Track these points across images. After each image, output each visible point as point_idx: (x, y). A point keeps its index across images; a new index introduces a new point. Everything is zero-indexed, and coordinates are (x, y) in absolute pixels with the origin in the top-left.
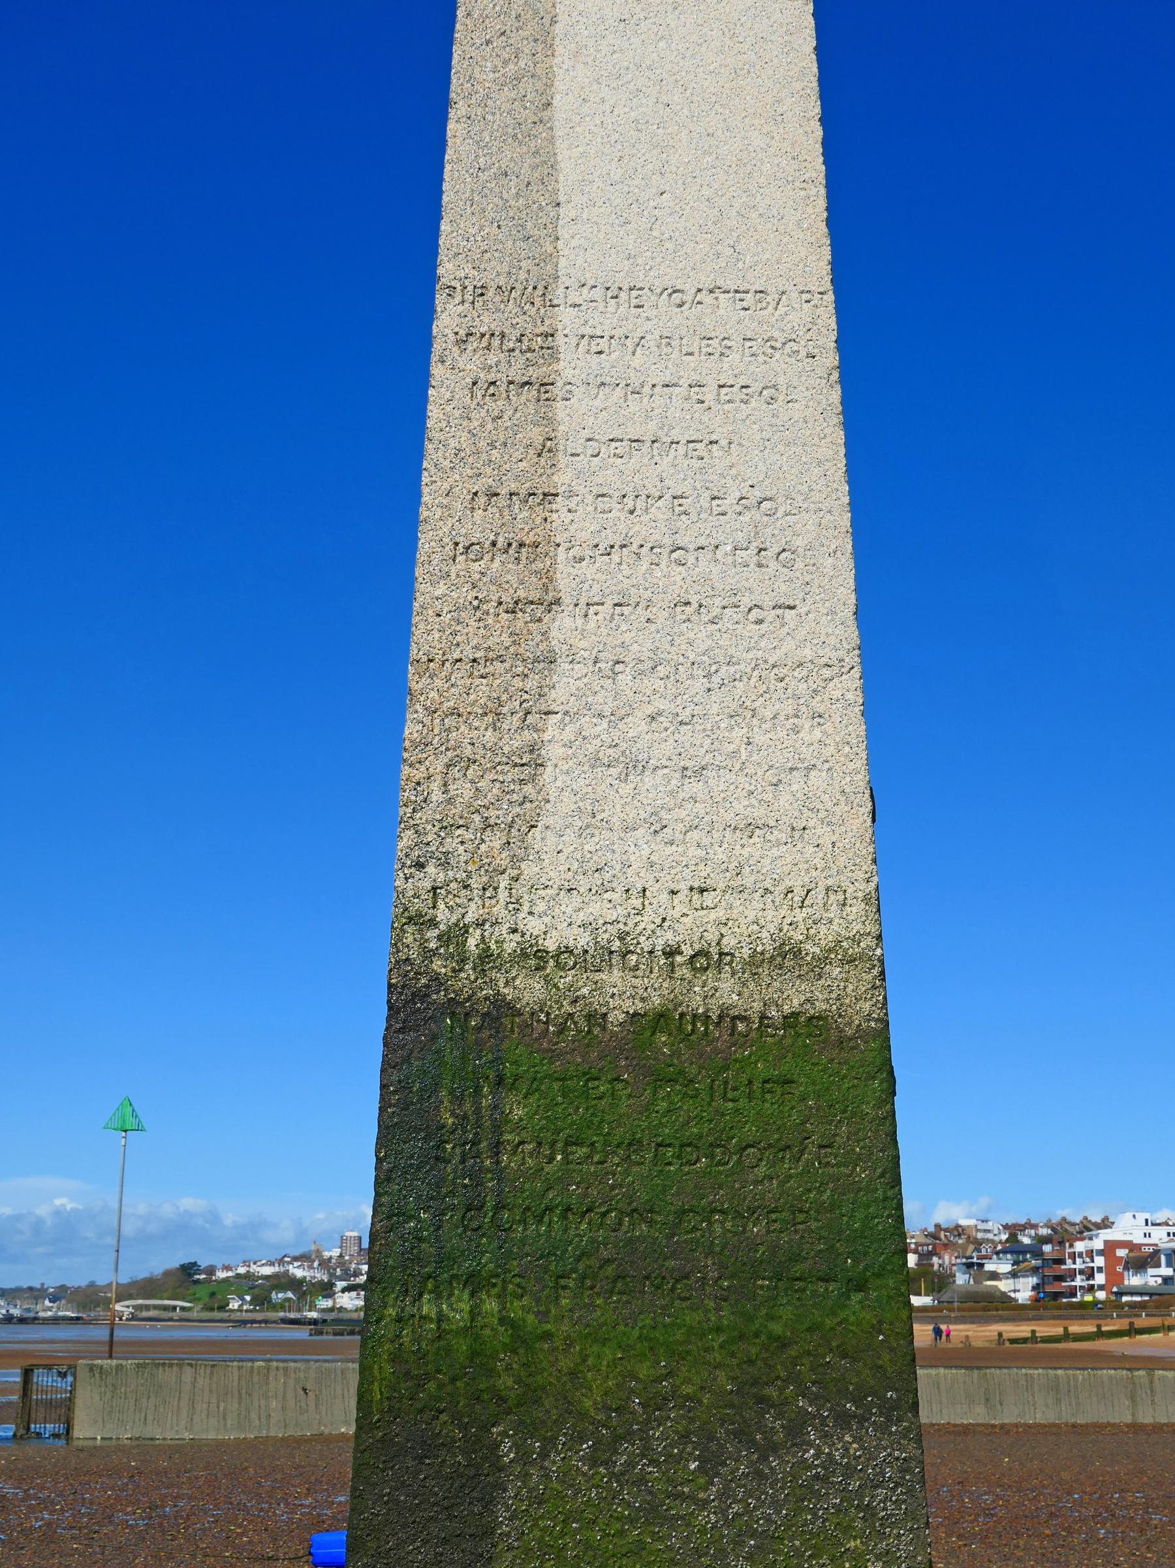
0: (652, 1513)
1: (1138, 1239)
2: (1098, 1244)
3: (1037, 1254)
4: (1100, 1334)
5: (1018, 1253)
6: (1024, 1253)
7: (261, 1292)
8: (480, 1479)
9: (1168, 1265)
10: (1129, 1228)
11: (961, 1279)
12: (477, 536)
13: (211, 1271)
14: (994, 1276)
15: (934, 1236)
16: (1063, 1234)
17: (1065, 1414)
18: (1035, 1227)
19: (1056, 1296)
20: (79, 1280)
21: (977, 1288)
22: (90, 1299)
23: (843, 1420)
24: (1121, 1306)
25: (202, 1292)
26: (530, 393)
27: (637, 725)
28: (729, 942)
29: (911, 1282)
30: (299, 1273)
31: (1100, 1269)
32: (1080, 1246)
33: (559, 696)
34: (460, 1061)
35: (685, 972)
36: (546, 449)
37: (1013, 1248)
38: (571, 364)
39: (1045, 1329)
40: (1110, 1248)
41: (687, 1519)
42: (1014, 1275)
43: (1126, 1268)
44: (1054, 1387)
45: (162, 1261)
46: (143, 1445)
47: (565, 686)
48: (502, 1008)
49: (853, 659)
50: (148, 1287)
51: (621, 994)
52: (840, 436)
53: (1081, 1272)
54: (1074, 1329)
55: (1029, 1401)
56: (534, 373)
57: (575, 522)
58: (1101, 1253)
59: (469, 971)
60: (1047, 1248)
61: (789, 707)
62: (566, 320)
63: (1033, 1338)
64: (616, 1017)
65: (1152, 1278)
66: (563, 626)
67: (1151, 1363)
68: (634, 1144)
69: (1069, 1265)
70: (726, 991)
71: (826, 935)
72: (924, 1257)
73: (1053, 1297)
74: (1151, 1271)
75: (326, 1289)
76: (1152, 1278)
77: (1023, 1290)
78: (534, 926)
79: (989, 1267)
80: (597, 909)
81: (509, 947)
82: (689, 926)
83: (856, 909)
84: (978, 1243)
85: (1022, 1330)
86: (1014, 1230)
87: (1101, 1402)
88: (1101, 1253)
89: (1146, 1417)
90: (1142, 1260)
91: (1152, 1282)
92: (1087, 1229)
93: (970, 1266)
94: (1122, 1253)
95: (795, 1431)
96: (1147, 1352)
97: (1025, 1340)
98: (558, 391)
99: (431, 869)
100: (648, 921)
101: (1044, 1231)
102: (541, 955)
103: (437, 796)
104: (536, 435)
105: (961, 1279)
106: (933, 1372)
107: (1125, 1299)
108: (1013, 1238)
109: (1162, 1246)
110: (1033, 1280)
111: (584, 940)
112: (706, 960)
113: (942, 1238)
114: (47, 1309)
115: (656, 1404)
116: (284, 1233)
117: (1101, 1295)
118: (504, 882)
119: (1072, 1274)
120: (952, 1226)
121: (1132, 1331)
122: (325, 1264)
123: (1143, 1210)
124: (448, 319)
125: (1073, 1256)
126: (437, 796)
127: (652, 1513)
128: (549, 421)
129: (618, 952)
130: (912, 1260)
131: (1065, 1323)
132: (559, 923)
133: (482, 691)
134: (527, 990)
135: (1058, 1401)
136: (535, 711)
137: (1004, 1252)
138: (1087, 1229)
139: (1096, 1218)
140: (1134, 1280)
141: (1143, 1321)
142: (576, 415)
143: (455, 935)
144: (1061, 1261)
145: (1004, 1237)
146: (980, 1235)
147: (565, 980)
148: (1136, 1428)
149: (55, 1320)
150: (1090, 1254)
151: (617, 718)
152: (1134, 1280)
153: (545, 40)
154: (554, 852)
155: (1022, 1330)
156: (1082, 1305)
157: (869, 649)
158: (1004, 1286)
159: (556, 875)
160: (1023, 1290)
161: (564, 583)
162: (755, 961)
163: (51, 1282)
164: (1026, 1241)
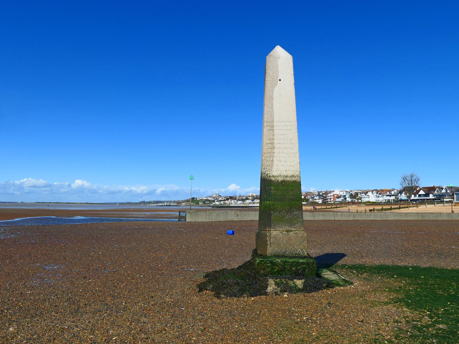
0: (283, 217)
1: (338, 194)
2: (332, 194)
3: (322, 196)
4: (332, 208)
7: (204, 202)
8: (270, 215)
10: (337, 192)
13: (196, 199)
14: (316, 199)
16: (326, 193)
19: (325, 202)
20: (177, 200)
22: (179, 203)
25: (195, 202)
27: (281, 158)
29: (303, 200)
30: (210, 199)
32: (329, 195)
33: (275, 156)
34: (266, 183)
36: (273, 135)
37: (319, 195)
38: (275, 128)
39: (323, 207)
40: (334, 195)
44: (323, 215)
45: (189, 197)
46: (196, 222)
47: (275, 155)
48: (271, 180)
50: (188, 201)
51: (280, 179)
54: (328, 207)
55: (319, 217)
57: (276, 141)
62: (275, 124)
63: (321, 208)
65: (340, 200)
66: (275, 150)
67: (337, 212)
68: (281, 190)
70: (288, 179)
71: (296, 174)
72: (305, 197)
73: (325, 202)
75: (214, 201)
76: (340, 200)
77: (320, 201)
80: (278, 172)
82: (285, 174)
84: (313, 194)
85: (320, 207)
86: (319, 192)
87: (330, 217)
89: (336, 219)
90: (339, 197)
92: (330, 192)
94: (336, 196)
95: (293, 211)
101: (324, 193)
105: (311, 200)
108: (319, 194)
112: (287, 176)
113: (307, 194)
114: (172, 204)
115: (283, 209)
116: (209, 193)
117: (332, 202)
119: (328, 199)
121: (337, 207)
122: (213, 197)
124: (265, 124)
127: (283, 217)
129: (280, 176)
130: (303, 197)
131: (382, 206)
132: (275, 174)
133: (269, 155)
134: (273, 179)
136: (273, 157)
138: (330, 192)
139: (332, 190)
140: (337, 200)
141: (338, 206)
142: (276, 132)
143: (267, 175)
148: (335, 220)
149: (174, 206)
151: (279, 157)
152: (337, 200)
153: (272, 99)
154: (275, 168)
155: (320, 207)
156: (329, 204)
158: (317, 201)
159: (275, 170)
160: (320, 201)
161: (275, 147)
163: (173, 200)
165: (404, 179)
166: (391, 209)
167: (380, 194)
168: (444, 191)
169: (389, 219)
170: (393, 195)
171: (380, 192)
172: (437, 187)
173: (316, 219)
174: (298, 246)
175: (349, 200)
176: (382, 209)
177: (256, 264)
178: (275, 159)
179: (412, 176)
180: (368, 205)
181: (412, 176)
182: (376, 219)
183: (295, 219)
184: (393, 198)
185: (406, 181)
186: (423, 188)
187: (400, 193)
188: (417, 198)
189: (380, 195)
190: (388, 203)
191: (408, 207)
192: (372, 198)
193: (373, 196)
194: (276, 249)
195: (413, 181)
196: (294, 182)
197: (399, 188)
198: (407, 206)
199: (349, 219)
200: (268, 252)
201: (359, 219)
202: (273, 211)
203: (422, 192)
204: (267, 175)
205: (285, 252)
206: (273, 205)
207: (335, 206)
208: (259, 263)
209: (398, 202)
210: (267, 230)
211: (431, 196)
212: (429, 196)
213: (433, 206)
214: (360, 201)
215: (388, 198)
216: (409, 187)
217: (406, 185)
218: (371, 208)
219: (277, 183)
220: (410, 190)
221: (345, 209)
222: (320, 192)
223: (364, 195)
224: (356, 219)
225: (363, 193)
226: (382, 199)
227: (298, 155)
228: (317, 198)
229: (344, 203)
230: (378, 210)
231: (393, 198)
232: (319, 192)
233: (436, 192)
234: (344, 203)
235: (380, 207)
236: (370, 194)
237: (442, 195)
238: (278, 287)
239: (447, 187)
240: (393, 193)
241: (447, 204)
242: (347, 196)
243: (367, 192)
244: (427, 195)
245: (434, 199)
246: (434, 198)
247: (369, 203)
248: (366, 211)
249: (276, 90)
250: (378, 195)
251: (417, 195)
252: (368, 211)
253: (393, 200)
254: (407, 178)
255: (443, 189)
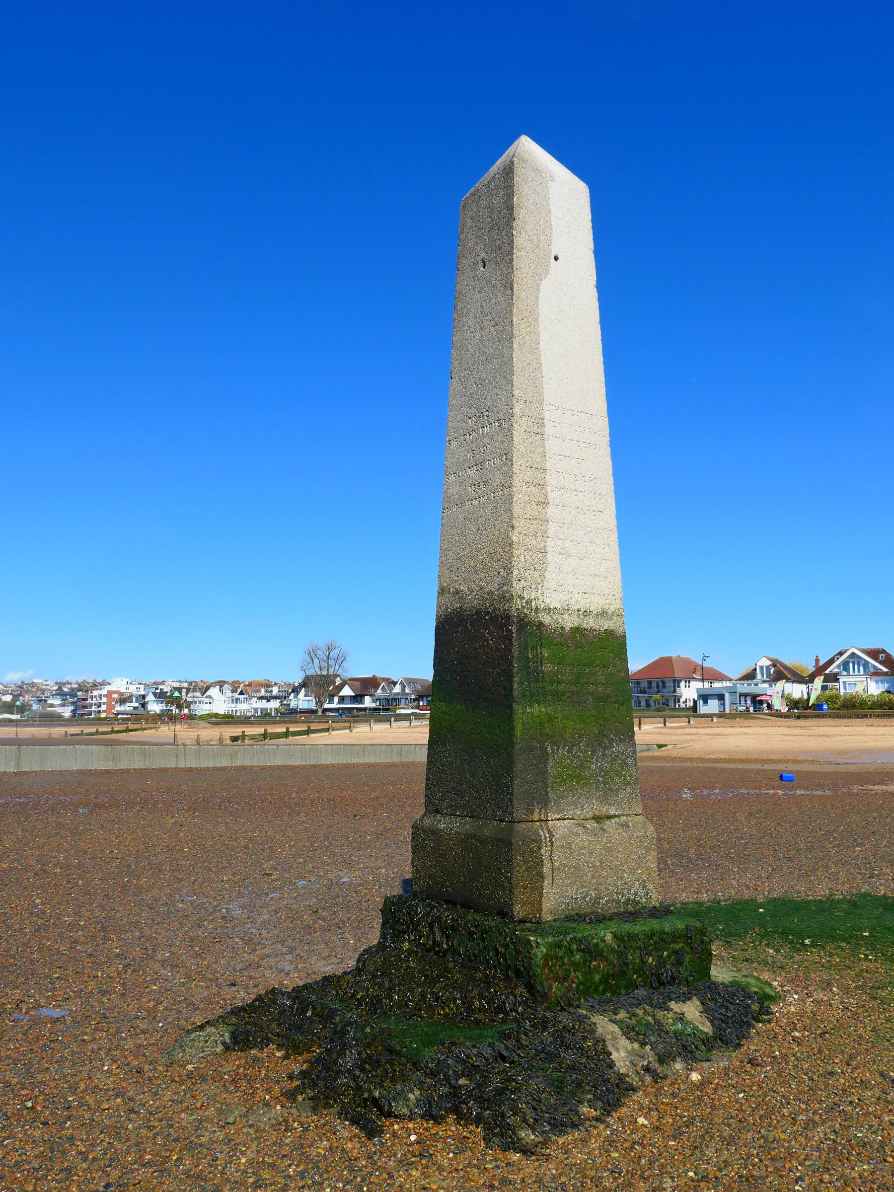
0: (581, 766)
1: (123, 690)
2: (104, 692)
4: (113, 732)
5: (63, 695)
6: (66, 695)
8: (544, 758)
9: (136, 701)
10: (119, 685)
11: (35, 707)
12: (528, 480)
14: (52, 706)
15: (21, 687)
16: (85, 688)
17: (148, 764)
18: (70, 683)
19: (83, 715)
21: (44, 711)
23: (621, 740)
24: (117, 720)
26: (539, 437)
27: (568, 543)
28: (592, 608)
31: (104, 703)
32: (95, 693)
33: (550, 533)
35: (582, 616)
37: (60, 693)
38: (549, 429)
40: (110, 693)
41: (589, 767)
42: (63, 705)
43: (116, 703)
44: (144, 753)
47: (552, 529)
48: (540, 624)
49: (616, 529)
51: (569, 622)
52: (611, 463)
53: (95, 704)
56: (539, 430)
57: (551, 479)
58: (105, 696)
59: (533, 613)
60: (80, 693)
61: (602, 542)
63: (82, 734)
64: (567, 628)
65: (128, 707)
66: (551, 511)
69: (90, 701)
70: (590, 623)
71: (613, 608)
73: (80, 715)
74: (128, 704)
76: (128, 707)
77: (67, 712)
78: (547, 601)
79: (49, 702)
80: (562, 597)
81: (542, 606)
82: (583, 605)
83: (619, 601)
84: (43, 691)
86: (60, 685)
88: (105, 696)
89: (182, 765)
90: (124, 700)
91: (128, 709)
92: (95, 686)
93: (40, 701)
94: (115, 696)
96: (136, 739)
97: (78, 735)
98: (546, 437)
99: (522, 581)
100: (573, 601)
102: (550, 609)
103: (523, 560)
104: (541, 450)
105: (35, 707)
106: (90, 747)
107: (120, 716)
108: (60, 688)
109: (134, 693)
110: (72, 708)
111: (559, 606)
112: (587, 613)
118: (540, 587)
119: (91, 705)
120: (30, 682)
121: (128, 730)
123: (126, 677)
125: (92, 697)
126: (523, 560)
127: (581, 766)
128: (544, 446)
129: (566, 610)
131: (288, 725)
134: (546, 619)
135: (145, 759)
137: (56, 695)
139: (99, 680)
140: (119, 708)
141: (131, 726)
142: (551, 445)
143: (529, 602)
144: (86, 699)
145: (56, 688)
146: (43, 687)
147: (555, 617)
150: (100, 696)
152: (119, 708)
153: (536, 320)
157: (619, 527)
158: (59, 710)
160: (67, 712)
162: (597, 615)
164: (66, 690)
165: (312, 654)
166: (286, 734)
167: (241, 693)
168: (397, 689)
169: (322, 761)
170: (275, 698)
171: (241, 690)
172: (383, 679)
173: (123, 765)
174: (632, 871)
175: (155, 707)
176: (265, 736)
177: (539, 961)
178: (550, 543)
179: (330, 649)
180: (217, 724)
181: (330, 649)
182: (290, 762)
183: (618, 774)
184: (275, 704)
185: (316, 661)
186: (350, 679)
187: (293, 691)
188: (335, 705)
189: (241, 697)
190: (265, 717)
191: (328, 730)
192: (220, 703)
193: (223, 698)
194: (571, 892)
195: (332, 662)
196: (609, 633)
197: (297, 680)
198: (325, 726)
199: (218, 765)
200: (547, 905)
201: (247, 763)
202: (554, 744)
203: (347, 691)
204: (529, 602)
205: (596, 901)
206: (551, 719)
207: (123, 727)
208: (546, 958)
209: (290, 714)
210: (536, 816)
211: (368, 702)
212: (362, 702)
213: (387, 725)
214: (186, 711)
215: (263, 704)
216: (321, 676)
217: (314, 670)
218: (237, 731)
219: (561, 635)
220: (320, 684)
221: (149, 734)
222: (65, 684)
223: (198, 694)
224: (238, 763)
225: (195, 691)
226: (244, 707)
227: (614, 537)
228: (57, 701)
229: (141, 717)
230: (253, 738)
231: (275, 704)
232: (60, 685)
233: (379, 691)
234: (141, 717)
235: (259, 730)
236: (214, 692)
237: (394, 700)
238: (643, 1044)
239: (406, 679)
240: (275, 690)
241: (418, 723)
242: (150, 698)
243: (208, 688)
244: (358, 698)
245: (375, 709)
246: (374, 705)
247: (215, 720)
248: (221, 740)
249: (547, 287)
250: (236, 695)
251: (336, 699)
252: (229, 742)
253: (276, 709)
254: (319, 652)
255: (395, 683)
